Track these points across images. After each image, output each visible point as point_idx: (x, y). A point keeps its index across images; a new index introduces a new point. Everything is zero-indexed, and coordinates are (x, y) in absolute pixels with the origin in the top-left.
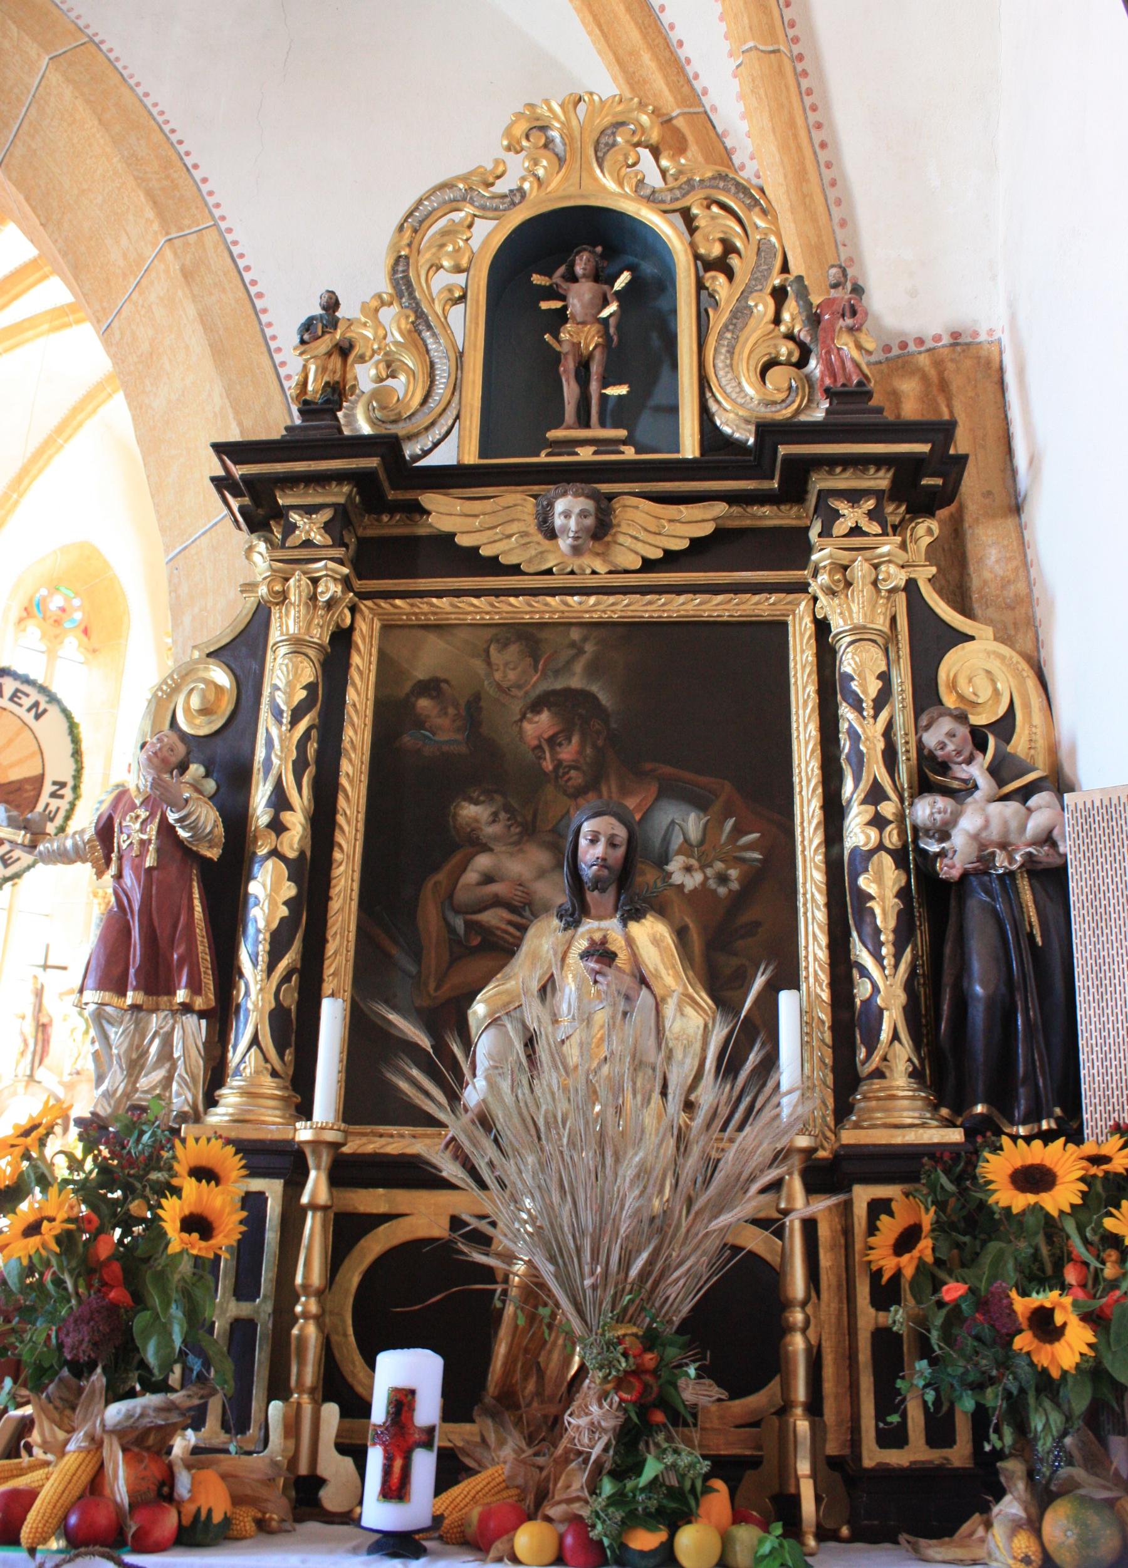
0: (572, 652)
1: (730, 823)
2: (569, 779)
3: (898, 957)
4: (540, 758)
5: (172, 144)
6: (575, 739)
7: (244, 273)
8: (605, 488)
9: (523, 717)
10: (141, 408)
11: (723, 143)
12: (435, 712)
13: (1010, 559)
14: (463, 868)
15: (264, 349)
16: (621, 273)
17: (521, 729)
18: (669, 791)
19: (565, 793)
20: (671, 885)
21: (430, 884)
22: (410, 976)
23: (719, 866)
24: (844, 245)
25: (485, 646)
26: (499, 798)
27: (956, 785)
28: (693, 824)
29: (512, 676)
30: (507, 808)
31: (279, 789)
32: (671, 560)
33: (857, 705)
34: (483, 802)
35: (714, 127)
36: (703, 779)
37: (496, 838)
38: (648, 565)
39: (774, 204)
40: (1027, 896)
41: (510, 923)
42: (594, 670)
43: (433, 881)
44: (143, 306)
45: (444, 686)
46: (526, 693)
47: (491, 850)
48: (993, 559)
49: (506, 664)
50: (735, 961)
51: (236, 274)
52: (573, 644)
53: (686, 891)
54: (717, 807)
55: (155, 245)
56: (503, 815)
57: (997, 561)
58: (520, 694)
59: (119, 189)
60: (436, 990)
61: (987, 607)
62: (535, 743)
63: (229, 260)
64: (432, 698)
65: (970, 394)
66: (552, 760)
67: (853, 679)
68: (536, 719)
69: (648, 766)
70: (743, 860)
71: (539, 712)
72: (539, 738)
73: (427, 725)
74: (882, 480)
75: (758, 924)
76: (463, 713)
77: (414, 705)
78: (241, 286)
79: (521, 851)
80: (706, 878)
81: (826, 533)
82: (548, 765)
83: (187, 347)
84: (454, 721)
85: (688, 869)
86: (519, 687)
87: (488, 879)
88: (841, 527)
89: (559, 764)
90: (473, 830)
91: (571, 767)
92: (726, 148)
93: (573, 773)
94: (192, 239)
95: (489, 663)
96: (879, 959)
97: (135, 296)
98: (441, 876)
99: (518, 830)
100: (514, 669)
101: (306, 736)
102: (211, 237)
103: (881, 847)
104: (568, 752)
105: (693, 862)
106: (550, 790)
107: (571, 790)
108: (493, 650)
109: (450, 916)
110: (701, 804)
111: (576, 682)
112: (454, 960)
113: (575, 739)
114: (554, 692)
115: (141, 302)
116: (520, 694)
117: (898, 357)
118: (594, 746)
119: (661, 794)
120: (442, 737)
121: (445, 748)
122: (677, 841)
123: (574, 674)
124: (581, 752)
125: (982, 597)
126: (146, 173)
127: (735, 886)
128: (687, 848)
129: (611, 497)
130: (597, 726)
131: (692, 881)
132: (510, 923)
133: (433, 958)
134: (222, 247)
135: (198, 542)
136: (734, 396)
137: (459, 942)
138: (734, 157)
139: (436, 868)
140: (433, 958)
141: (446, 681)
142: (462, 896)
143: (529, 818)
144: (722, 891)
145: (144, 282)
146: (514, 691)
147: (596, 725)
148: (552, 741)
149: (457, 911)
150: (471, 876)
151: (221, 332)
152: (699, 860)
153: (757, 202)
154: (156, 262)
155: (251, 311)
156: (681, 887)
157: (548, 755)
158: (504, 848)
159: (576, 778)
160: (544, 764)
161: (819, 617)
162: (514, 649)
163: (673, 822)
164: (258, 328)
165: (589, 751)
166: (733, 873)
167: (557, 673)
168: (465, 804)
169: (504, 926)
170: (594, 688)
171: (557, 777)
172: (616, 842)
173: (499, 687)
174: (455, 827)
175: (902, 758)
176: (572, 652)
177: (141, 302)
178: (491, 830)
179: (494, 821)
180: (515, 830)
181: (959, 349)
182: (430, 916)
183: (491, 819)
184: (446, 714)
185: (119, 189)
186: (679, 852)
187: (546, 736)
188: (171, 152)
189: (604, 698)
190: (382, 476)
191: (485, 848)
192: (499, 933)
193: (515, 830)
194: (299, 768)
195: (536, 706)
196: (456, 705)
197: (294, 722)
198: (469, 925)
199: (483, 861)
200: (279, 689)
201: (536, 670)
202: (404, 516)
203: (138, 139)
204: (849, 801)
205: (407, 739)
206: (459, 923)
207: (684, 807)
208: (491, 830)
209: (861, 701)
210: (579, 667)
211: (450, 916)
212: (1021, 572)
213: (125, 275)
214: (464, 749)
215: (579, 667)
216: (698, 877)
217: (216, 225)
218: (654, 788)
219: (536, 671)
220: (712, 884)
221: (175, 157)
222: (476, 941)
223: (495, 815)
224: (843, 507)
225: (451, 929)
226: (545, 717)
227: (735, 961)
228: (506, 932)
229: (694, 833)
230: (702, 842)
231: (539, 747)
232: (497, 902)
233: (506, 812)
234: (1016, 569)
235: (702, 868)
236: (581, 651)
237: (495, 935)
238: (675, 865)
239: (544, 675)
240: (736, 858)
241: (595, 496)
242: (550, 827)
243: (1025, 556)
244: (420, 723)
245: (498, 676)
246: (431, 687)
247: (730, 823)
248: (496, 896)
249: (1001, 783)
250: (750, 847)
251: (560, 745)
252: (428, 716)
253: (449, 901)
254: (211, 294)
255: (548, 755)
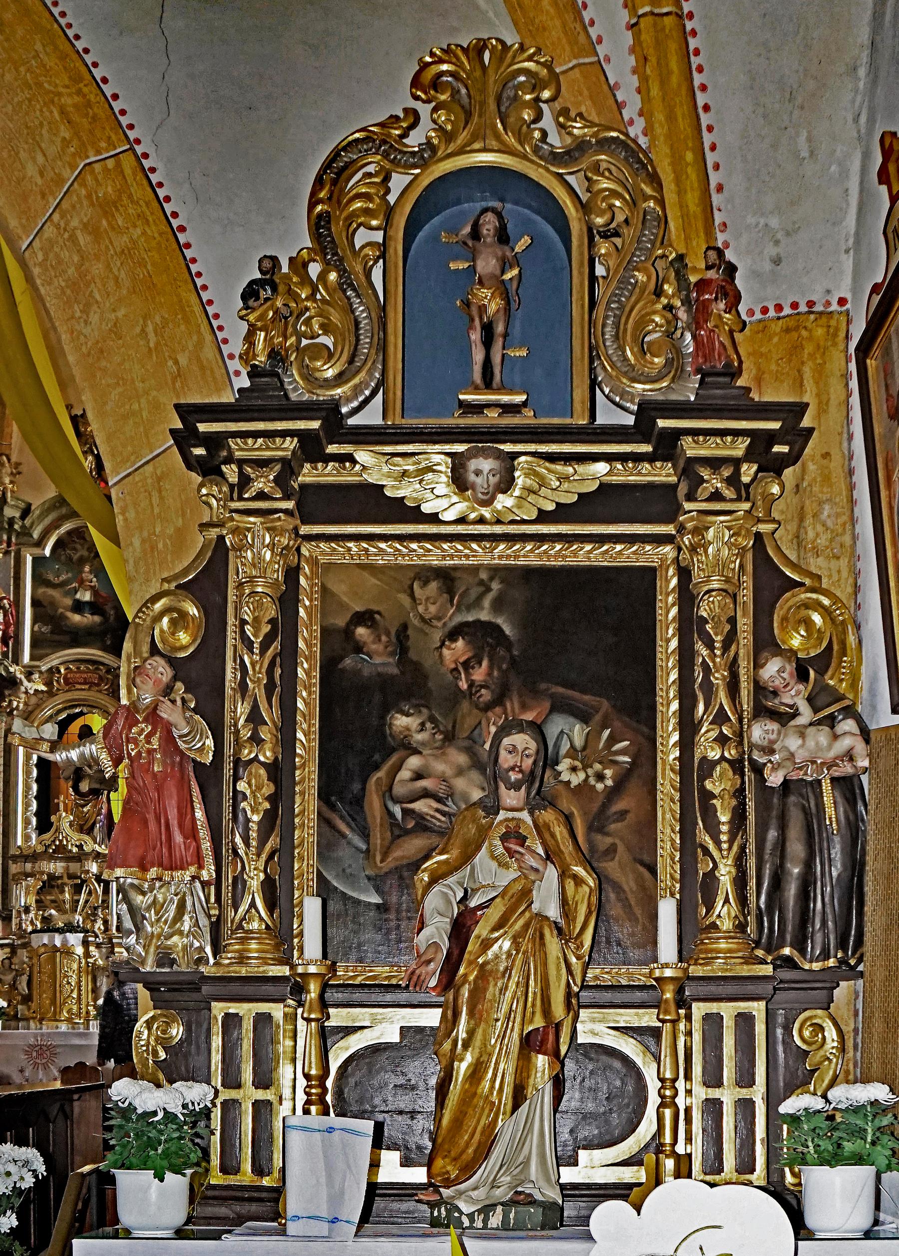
0: (482, 589)
1: (606, 733)
2: (481, 696)
3: (731, 842)
4: (457, 678)
5: (78, 52)
6: (485, 663)
7: (165, 205)
8: (508, 447)
9: (443, 644)
10: (72, 332)
11: (614, 96)
12: (371, 638)
13: (838, 515)
14: (398, 767)
15: (191, 286)
16: (522, 237)
17: (441, 655)
18: (560, 707)
19: (477, 707)
20: (561, 781)
21: (373, 779)
22: (361, 851)
23: (598, 767)
24: (719, 210)
25: (409, 583)
26: (425, 711)
27: (783, 709)
28: (578, 733)
29: (433, 609)
30: (432, 719)
31: (255, 708)
32: (562, 513)
33: (710, 644)
34: (412, 715)
35: (607, 79)
36: (587, 698)
37: (423, 744)
38: (543, 517)
39: (659, 170)
40: (828, 800)
41: (437, 810)
42: (498, 605)
43: (375, 778)
44: (65, 230)
45: (377, 616)
46: (445, 624)
47: (420, 753)
48: (826, 513)
49: (427, 599)
50: (609, 840)
51: (157, 204)
52: (481, 583)
53: (572, 786)
54: (598, 718)
55: (73, 167)
56: (428, 725)
57: (829, 516)
58: (440, 624)
59: (30, 100)
60: (382, 861)
61: (818, 556)
62: (453, 666)
63: (149, 189)
64: (368, 627)
65: (819, 361)
66: (467, 681)
67: (707, 622)
68: (453, 646)
69: (543, 686)
70: (615, 763)
71: (455, 641)
72: (456, 662)
73: (365, 650)
74: (740, 448)
75: (626, 812)
76: (394, 640)
77: (353, 633)
78: (163, 218)
79: (443, 754)
80: (587, 777)
81: (690, 497)
82: (463, 685)
83: (116, 279)
84: (386, 647)
85: (574, 769)
86: (439, 619)
87: (418, 776)
88: (704, 491)
89: (471, 684)
90: (406, 737)
91: (482, 687)
92: (616, 101)
93: (483, 691)
94: (110, 163)
95: (412, 595)
96: (718, 843)
97: (56, 217)
98: (381, 774)
99: (441, 737)
100: (434, 603)
101: (272, 664)
102: (128, 162)
103: (723, 758)
104: (479, 674)
105: (578, 764)
106: (465, 705)
107: (482, 705)
108: (416, 586)
109: (390, 804)
110: (584, 718)
111: (484, 616)
112: (395, 838)
113: (485, 663)
114: (467, 624)
115: (62, 224)
116: (440, 624)
117: (760, 321)
118: (500, 668)
119: (553, 709)
120: (378, 660)
121: (380, 669)
122: (565, 747)
123: (482, 609)
124: (489, 674)
125: (814, 548)
126: (56, 86)
127: (609, 783)
128: (573, 752)
129: (515, 455)
130: (502, 653)
131: (576, 779)
132: (437, 810)
133: (378, 839)
134: (140, 175)
135: (141, 470)
136: (619, 365)
137: (398, 825)
138: (624, 112)
139: (377, 767)
140: (378, 839)
141: (379, 613)
142: (399, 790)
143: (450, 728)
144: (600, 786)
145: (65, 205)
146: (435, 623)
147: (502, 652)
148: (466, 665)
149: (396, 801)
150: (405, 774)
151: (149, 267)
152: (582, 762)
153: (644, 166)
154: (76, 184)
155: (175, 246)
156: (568, 783)
157: (463, 676)
158: (430, 752)
159: (486, 695)
160: (460, 684)
161: (682, 565)
162: (434, 585)
163: (562, 732)
164: (183, 266)
165: (496, 673)
166: (608, 773)
167: (469, 608)
168: (398, 716)
169: (432, 813)
170: (500, 621)
171: (471, 694)
172: (890, 1153)
173: (423, 619)
174: (391, 734)
175: (743, 685)
176: (482, 589)
177: (62, 224)
178: (419, 737)
179: (422, 730)
180: (439, 737)
181: (812, 317)
182: (374, 803)
183: (419, 728)
184: (380, 640)
185: (30, 100)
186: (565, 757)
187: (462, 660)
188: (79, 64)
189: (507, 630)
190: (324, 441)
191: (416, 752)
192: (428, 818)
193: (439, 737)
194: (270, 689)
195: (453, 635)
196: (388, 634)
197: (262, 653)
198: (405, 812)
199: (414, 762)
200: (247, 623)
201: (452, 605)
202: (337, 465)
203: (44, 46)
204: (701, 721)
205: (348, 662)
206: (397, 810)
207: (572, 720)
208: (419, 737)
209: (713, 641)
210: (487, 602)
211: (390, 804)
212: (848, 527)
213: (43, 195)
214: (395, 671)
215: (487, 602)
216: (582, 776)
217: (132, 149)
218: (547, 705)
219: (452, 605)
220: (592, 781)
221: (83, 69)
222: (411, 825)
223: (423, 724)
224: (705, 473)
225: (391, 815)
226: (460, 643)
227: (609, 840)
228: (433, 817)
229: (579, 742)
230: (584, 748)
231: (456, 669)
232: (426, 794)
233: (432, 723)
234: (844, 524)
235: (584, 768)
236: (489, 589)
237: (424, 819)
238: (564, 766)
239: (458, 609)
240: (611, 761)
241: (500, 455)
242: (466, 735)
243: (852, 511)
244: (358, 648)
245: (421, 609)
246: (365, 618)
247: (606, 733)
248: (425, 789)
249: (816, 711)
250: (622, 752)
251: (473, 668)
252: (365, 643)
253: (388, 792)
254: (135, 226)
255: (463, 676)
